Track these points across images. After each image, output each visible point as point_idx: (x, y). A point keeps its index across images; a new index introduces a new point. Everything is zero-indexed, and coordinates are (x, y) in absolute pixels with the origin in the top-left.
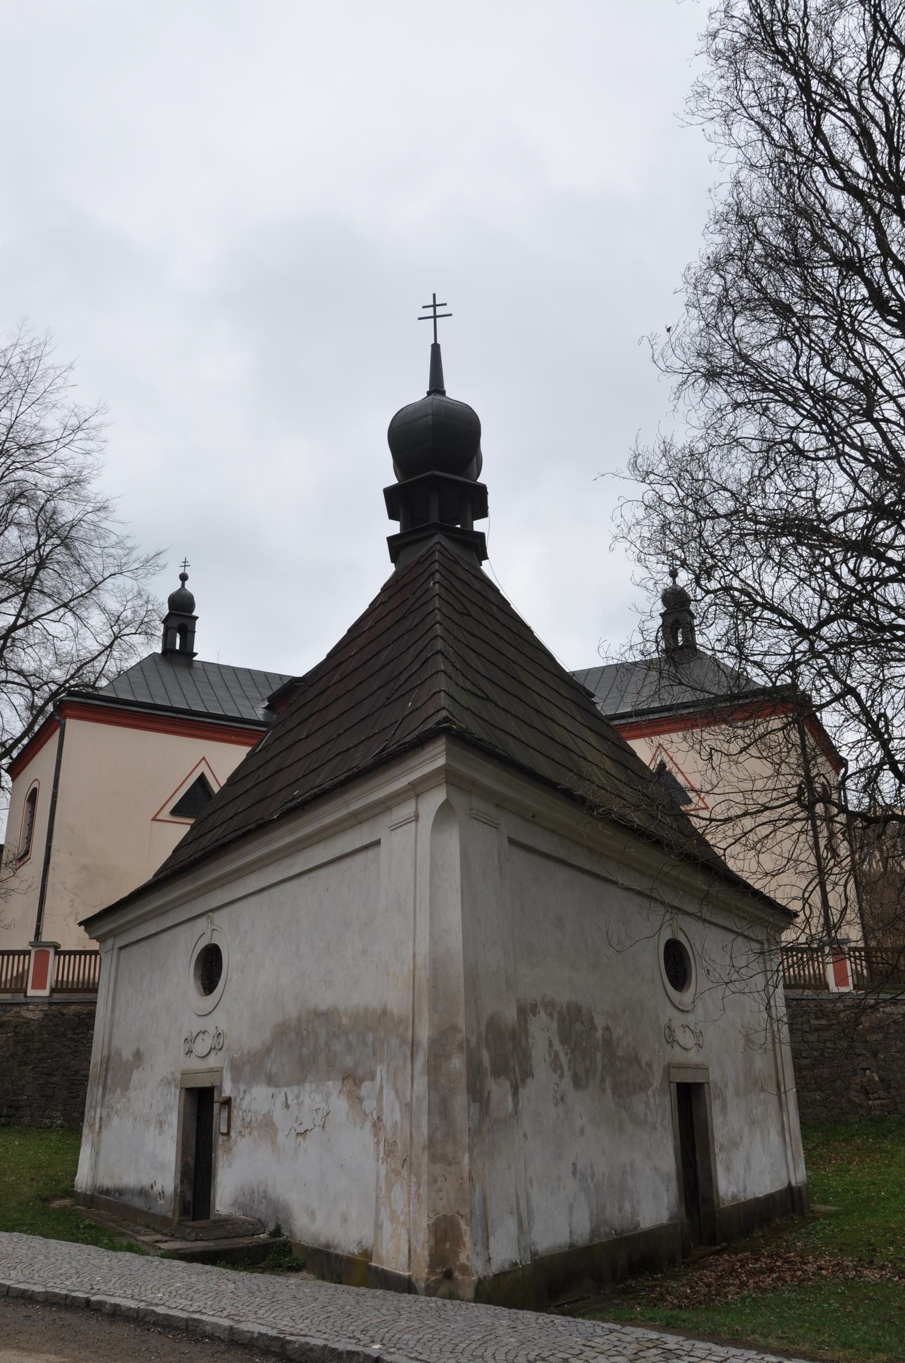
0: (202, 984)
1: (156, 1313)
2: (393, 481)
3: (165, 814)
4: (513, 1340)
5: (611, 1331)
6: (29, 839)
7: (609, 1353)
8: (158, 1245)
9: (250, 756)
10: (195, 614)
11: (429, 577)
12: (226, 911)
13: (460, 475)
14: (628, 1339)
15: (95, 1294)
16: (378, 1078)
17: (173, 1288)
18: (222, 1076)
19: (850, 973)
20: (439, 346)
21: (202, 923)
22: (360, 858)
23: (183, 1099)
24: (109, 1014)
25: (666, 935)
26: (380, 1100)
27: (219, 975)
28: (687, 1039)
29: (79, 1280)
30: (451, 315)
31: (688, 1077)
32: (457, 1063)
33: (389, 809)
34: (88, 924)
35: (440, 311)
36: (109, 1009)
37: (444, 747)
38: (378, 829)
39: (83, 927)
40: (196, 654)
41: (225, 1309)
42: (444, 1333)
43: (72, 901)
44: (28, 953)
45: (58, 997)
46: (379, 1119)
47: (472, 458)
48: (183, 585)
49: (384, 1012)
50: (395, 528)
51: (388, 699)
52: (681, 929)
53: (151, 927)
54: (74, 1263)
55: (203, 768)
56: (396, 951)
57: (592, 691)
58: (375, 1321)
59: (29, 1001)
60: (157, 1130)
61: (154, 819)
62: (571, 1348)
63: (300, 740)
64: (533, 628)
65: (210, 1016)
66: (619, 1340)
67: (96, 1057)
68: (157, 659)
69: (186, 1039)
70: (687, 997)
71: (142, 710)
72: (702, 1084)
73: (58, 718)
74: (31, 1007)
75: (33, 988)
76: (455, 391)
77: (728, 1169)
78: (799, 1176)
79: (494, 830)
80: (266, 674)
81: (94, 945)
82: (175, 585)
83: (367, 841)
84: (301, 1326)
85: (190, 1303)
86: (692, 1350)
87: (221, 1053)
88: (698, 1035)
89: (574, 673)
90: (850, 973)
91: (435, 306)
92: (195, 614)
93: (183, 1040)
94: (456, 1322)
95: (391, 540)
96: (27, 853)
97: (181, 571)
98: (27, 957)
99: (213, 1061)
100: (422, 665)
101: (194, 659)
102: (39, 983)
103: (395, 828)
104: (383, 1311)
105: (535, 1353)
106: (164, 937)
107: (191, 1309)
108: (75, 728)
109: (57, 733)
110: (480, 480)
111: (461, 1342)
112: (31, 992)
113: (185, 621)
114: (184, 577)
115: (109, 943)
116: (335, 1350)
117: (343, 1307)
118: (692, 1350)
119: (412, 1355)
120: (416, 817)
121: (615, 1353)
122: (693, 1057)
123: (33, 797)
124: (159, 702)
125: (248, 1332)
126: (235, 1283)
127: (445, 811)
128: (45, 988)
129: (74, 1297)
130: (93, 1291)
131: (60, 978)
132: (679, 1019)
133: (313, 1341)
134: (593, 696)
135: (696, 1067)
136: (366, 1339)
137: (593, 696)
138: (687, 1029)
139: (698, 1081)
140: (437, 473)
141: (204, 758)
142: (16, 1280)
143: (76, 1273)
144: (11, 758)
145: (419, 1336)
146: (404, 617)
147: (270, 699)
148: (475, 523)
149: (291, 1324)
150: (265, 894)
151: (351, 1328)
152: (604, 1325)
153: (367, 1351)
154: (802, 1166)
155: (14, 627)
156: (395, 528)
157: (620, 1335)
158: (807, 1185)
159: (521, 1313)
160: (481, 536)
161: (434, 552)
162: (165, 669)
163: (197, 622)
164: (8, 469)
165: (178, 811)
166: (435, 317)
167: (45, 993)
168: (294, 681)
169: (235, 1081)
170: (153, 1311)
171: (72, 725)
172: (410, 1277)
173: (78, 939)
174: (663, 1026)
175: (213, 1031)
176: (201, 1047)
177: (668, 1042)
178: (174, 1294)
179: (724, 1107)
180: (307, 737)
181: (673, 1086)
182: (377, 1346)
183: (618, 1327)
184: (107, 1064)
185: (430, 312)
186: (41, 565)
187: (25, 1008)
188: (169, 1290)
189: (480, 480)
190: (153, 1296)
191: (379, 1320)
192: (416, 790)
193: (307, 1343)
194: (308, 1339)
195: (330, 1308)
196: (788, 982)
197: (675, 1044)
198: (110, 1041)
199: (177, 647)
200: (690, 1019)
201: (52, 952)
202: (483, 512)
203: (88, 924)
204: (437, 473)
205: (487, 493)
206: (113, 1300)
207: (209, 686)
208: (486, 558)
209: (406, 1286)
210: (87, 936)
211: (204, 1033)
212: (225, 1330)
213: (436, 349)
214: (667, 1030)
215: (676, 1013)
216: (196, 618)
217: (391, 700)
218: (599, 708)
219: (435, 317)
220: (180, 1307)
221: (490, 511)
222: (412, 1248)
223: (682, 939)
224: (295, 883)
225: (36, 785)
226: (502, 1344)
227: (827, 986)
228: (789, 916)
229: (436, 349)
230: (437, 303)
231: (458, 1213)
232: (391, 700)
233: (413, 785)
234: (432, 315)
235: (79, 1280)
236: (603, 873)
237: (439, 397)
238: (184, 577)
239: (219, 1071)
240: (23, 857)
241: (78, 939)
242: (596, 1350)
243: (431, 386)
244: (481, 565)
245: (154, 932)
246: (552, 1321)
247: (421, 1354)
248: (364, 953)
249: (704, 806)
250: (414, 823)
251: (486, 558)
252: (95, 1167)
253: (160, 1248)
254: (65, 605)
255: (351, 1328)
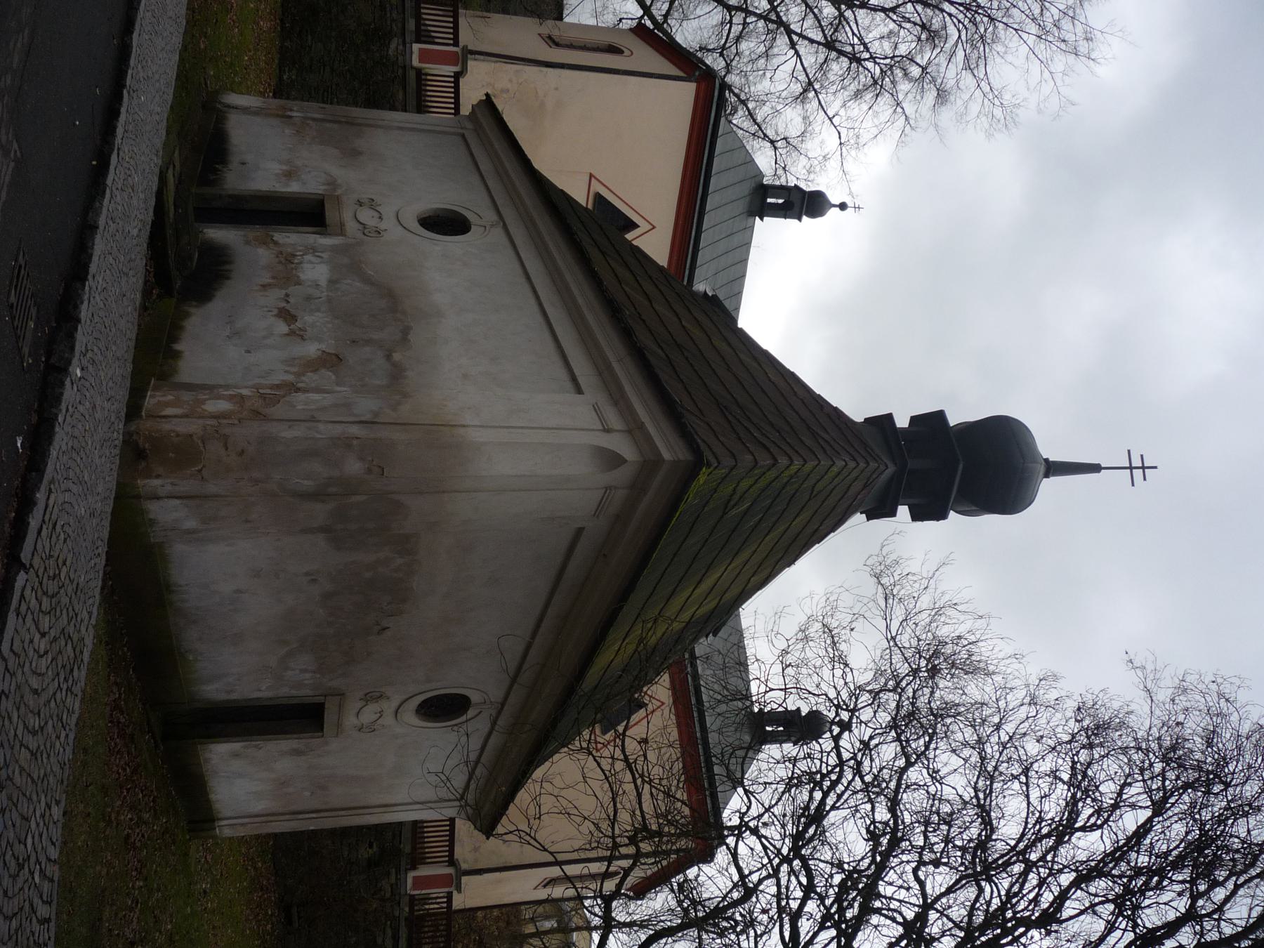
0: (430, 216)
1: (112, 153)
2: (953, 420)
3: (597, 187)
4: (83, 512)
5: (90, 613)
6: (571, 46)
7: (70, 609)
8: (172, 166)
9: (661, 268)
10: (805, 218)
11: (853, 457)
12: (504, 240)
13: (958, 491)
14: (83, 629)
15: (129, 93)
16: (338, 389)
17: (133, 172)
18: (337, 235)
19: (423, 892)
20: (1099, 472)
21: (490, 216)
22: (562, 374)
23: (312, 197)
24: (396, 124)
25: (475, 697)
26: (318, 390)
27: (438, 233)
28: (368, 715)
29: (142, 79)
30: (1133, 485)
31: (329, 717)
32: (354, 467)
33: (616, 404)
34: (488, 103)
35: (1138, 474)
36: (401, 125)
37: (682, 458)
38: (593, 393)
39: (484, 98)
40: (762, 219)
41: (114, 223)
42: (90, 443)
43: (508, 91)
44: (456, 44)
45: (412, 75)
46: (298, 390)
47: (977, 506)
48: (835, 206)
49: (406, 395)
50: (902, 422)
51: (725, 407)
52: (480, 712)
53: (485, 166)
54: (157, 77)
55: (644, 226)
56: (469, 408)
57: (720, 634)
58: (102, 374)
59: (408, 45)
60: (280, 172)
61: (591, 176)
62: (76, 571)
63: (680, 319)
64: (793, 567)
65: (398, 223)
66: (82, 620)
67: (358, 113)
68: (757, 179)
69: (373, 200)
70: (410, 717)
71: (705, 161)
72: (322, 730)
73: (697, 74)
74: (401, 47)
75: (420, 50)
76: (1049, 488)
77: (236, 755)
78: (225, 830)
79: (593, 513)
80: (740, 293)
81: (465, 110)
82: (834, 198)
83: (581, 380)
84: (98, 298)
85: (120, 188)
86: (72, 693)
87: (360, 235)
88: (371, 729)
89: (738, 615)
90: (423, 892)
91: (1143, 468)
92: (805, 218)
93: (373, 197)
94: (100, 457)
95: (889, 418)
96: (557, 44)
97: (850, 204)
98: (451, 42)
99: (351, 226)
100: (761, 443)
101: (757, 218)
102: (425, 57)
103: (596, 409)
104: (111, 384)
105: (71, 533)
106: (475, 179)
107: (114, 189)
108: (687, 91)
109: (681, 74)
110: (952, 513)
111: (82, 459)
112: (416, 47)
113: (796, 209)
114: (843, 206)
115: (469, 125)
116: (76, 329)
117: (115, 343)
118: (72, 693)
119: (70, 407)
120: (607, 430)
121: (70, 615)
122: (350, 720)
123: (613, 50)
124: (713, 180)
125: (93, 244)
126: (137, 236)
127: (612, 460)
128: (420, 61)
129: (127, 72)
130: (131, 92)
131: (429, 77)
132: (389, 706)
133: (84, 307)
134: (715, 635)
135: (339, 725)
136: (84, 362)
137: (715, 635)
138: (379, 715)
139: (325, 726)
140: (961, 467)
141: (654, 227)
142: (144, 16)
143: (148, 77)
144: (654, 29)
145: (87, 417)
146: (809, 428)
147: (715, 297)
148: (907, 507)
149: (99, 287)
150: (523, 280)
151: (95, 349)
152: (95, 607)
153: (75, 361)
154: (241, 832)
155: (789, 32)
156: (902, 422)
157: (86, 622)
158: (214, 837)
159: (107, 523)
160: (892, 513)
161: (877, 461)
162: (746, 188)
163: (796, 221)
164: (959, 21)
165: (599, 198)
166: (1131, 468)
167: (415, 62)
168: (735, 321)
169: (335, 249)
170: (113, 150)
171: (687, 91)
172: (141, 417)
173: (471, 95)
174: (383, 690)
175: (382, 226)
176: (366, 216)
177: (366, 695)
178: (128, 173)
179: (297, 752)
180: (683, 327)
181: (321, 699)
182: (79, 373)
183: (93, 621)
184: (347, 123)
185: (1136, 462)
186: (855, 59)
187: (400, 40)
188: (131, 168)
189: (952, 513)
190: (126, 151)
191: (102, 378)
192: (635, 429)
193: (82, 303)
194: (86, 303)
195: (113, 330)
196: (419, 825)
197: (364, 703)
198: (372, 126)
199: (769, 200)
200: (388, 720)
201: (457, 69)
202: (917, 516)
203: (488, 103)
204: (961, 467)
205: (938, 520)
206: (123, 110)
207: (728, 233)
208: (868, 519)
209: (133, 410)
210: (475, 103)
211: (380, 218)
212: (95, 222)
213: (1095, 468)
214: (378, 694)
215: (395, 704)
216: (800, 219)
217: (724, 410)
218: (701, 641)
219: (1131, 468)
220: (116, 178)
221: (919, 524)
222: (170, 419)
223: (471, 713)
224: (536, 308)
225: (627, 52)
226: (79, 500)
227: (414, 868)
228: (488, 829)
229: (1095, 468)
230: (1146, 470)
231: (204, 466)
232: (724, 410)
233: (641, 427)
234: (1133, 465)
235: (142, 79)
236: (541, 630)
237: (1042, 469)
238: (843, 206)
239: (341, 231)
240: (552, 41)
241: (471, 95)
242: (73, 597)
243: (1054, 463)
244: (861, 513)
245: (481, 167)
246: (99, 554)
247: (71, 416)
248: (465, 376)
249: (659, 704)
250: (601, 428)
251: (868, 519)
252: (245, 110)
253: (168, 168)
254: (810, 84)
255: (95, 349)
